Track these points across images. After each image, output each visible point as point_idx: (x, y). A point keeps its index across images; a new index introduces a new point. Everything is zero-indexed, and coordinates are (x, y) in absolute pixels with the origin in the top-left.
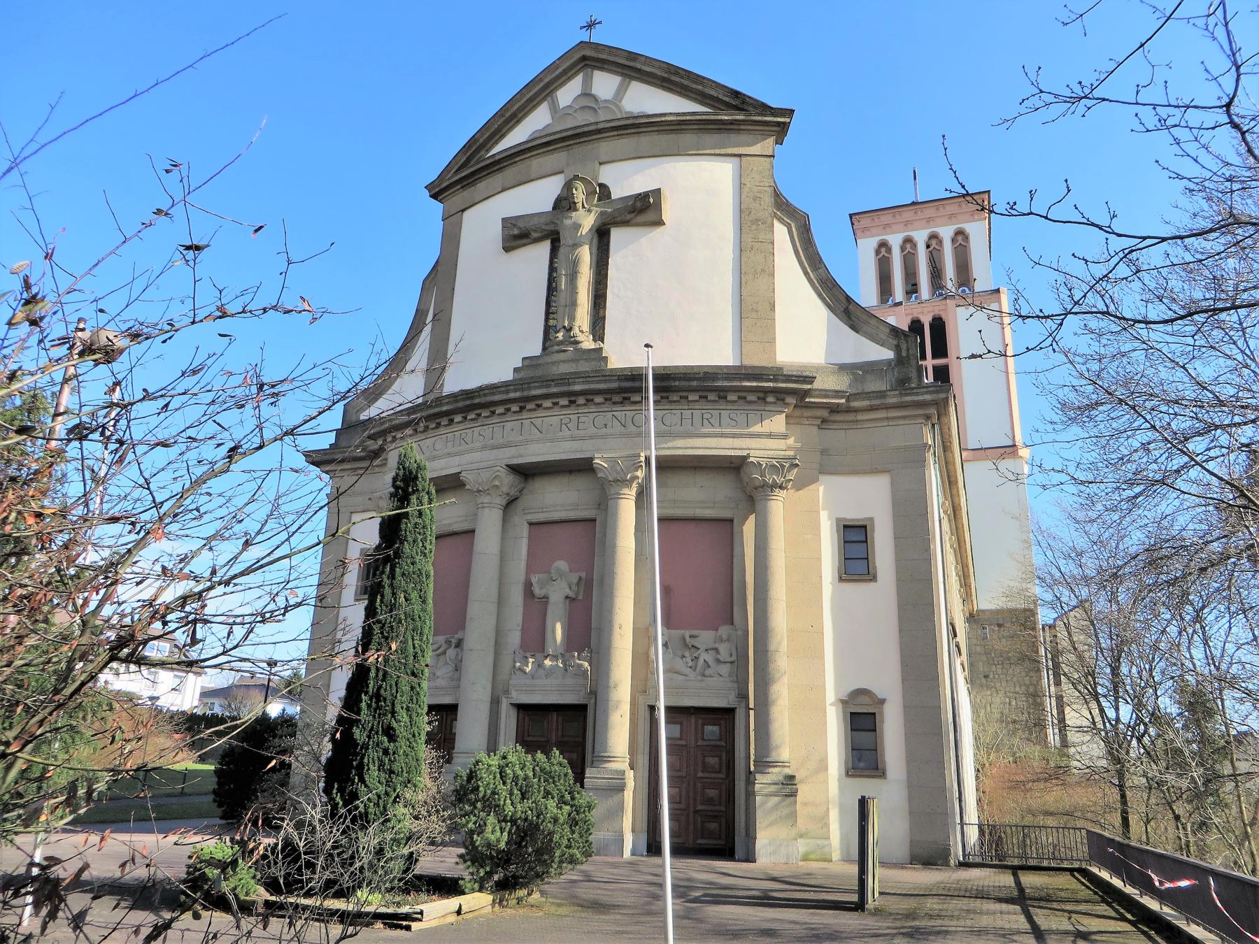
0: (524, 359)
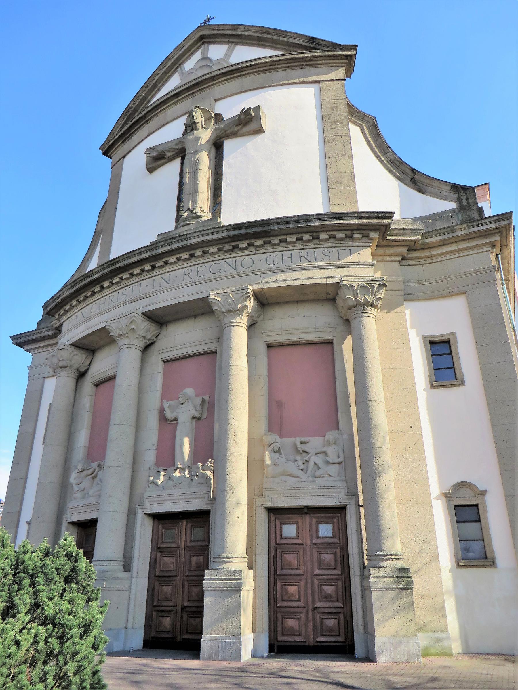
0: (158, 235)
